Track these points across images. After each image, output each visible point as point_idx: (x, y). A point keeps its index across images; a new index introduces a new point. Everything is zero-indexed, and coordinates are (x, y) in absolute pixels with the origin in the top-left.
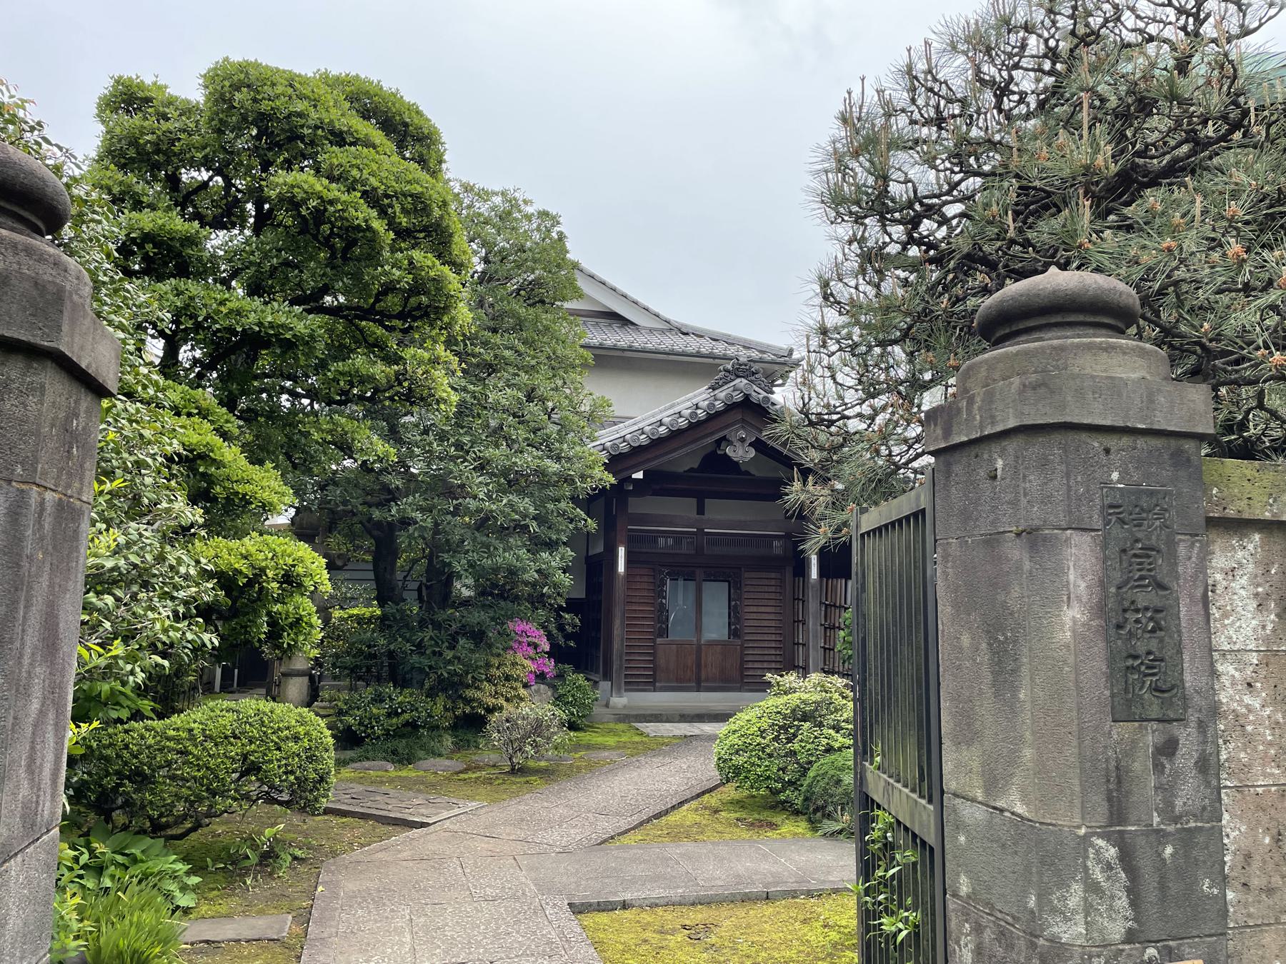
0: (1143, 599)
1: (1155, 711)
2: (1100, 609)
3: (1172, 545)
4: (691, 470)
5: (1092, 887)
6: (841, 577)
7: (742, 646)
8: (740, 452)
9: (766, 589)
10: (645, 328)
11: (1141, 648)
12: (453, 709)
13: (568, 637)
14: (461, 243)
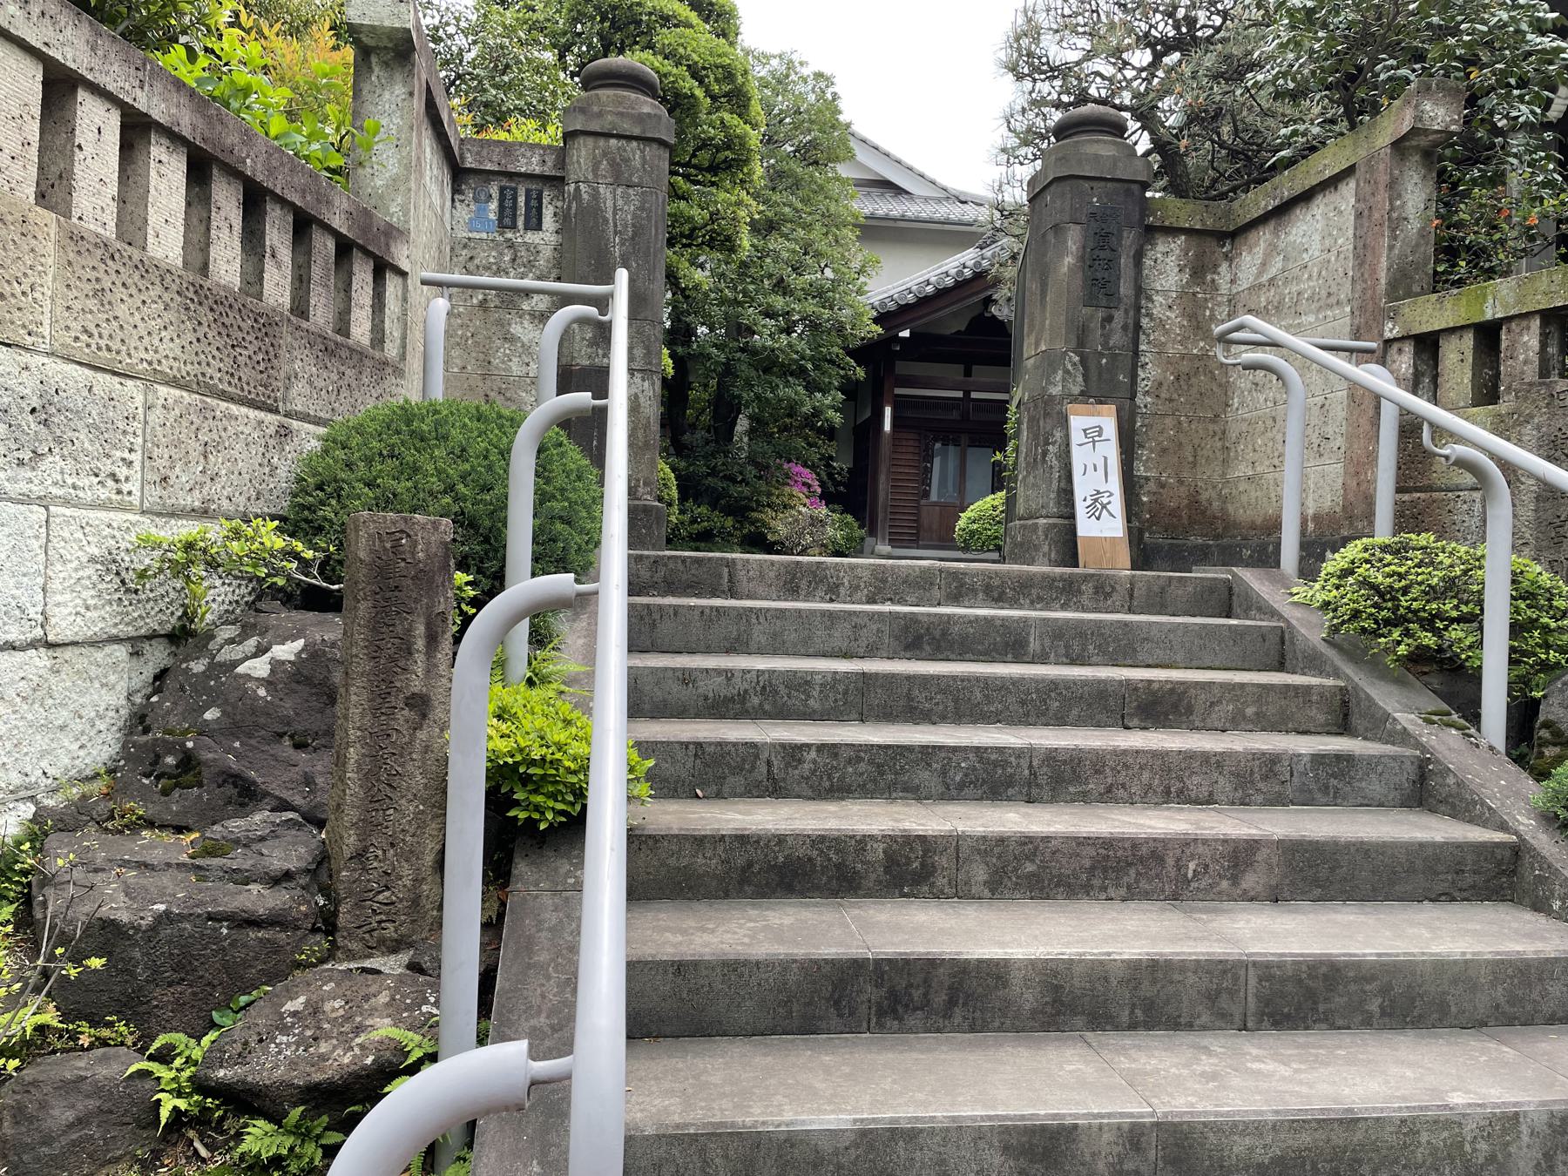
0: (1102, 254)
1: (1104, 303)
2: (1082, 258)
3: (1120, 231)
4: (959, 332)
5: (1067, 372)
10: (920, 197)
11: (1099, 275)
12: (742, 527)
13: (837, 484)
14: (756, 108)
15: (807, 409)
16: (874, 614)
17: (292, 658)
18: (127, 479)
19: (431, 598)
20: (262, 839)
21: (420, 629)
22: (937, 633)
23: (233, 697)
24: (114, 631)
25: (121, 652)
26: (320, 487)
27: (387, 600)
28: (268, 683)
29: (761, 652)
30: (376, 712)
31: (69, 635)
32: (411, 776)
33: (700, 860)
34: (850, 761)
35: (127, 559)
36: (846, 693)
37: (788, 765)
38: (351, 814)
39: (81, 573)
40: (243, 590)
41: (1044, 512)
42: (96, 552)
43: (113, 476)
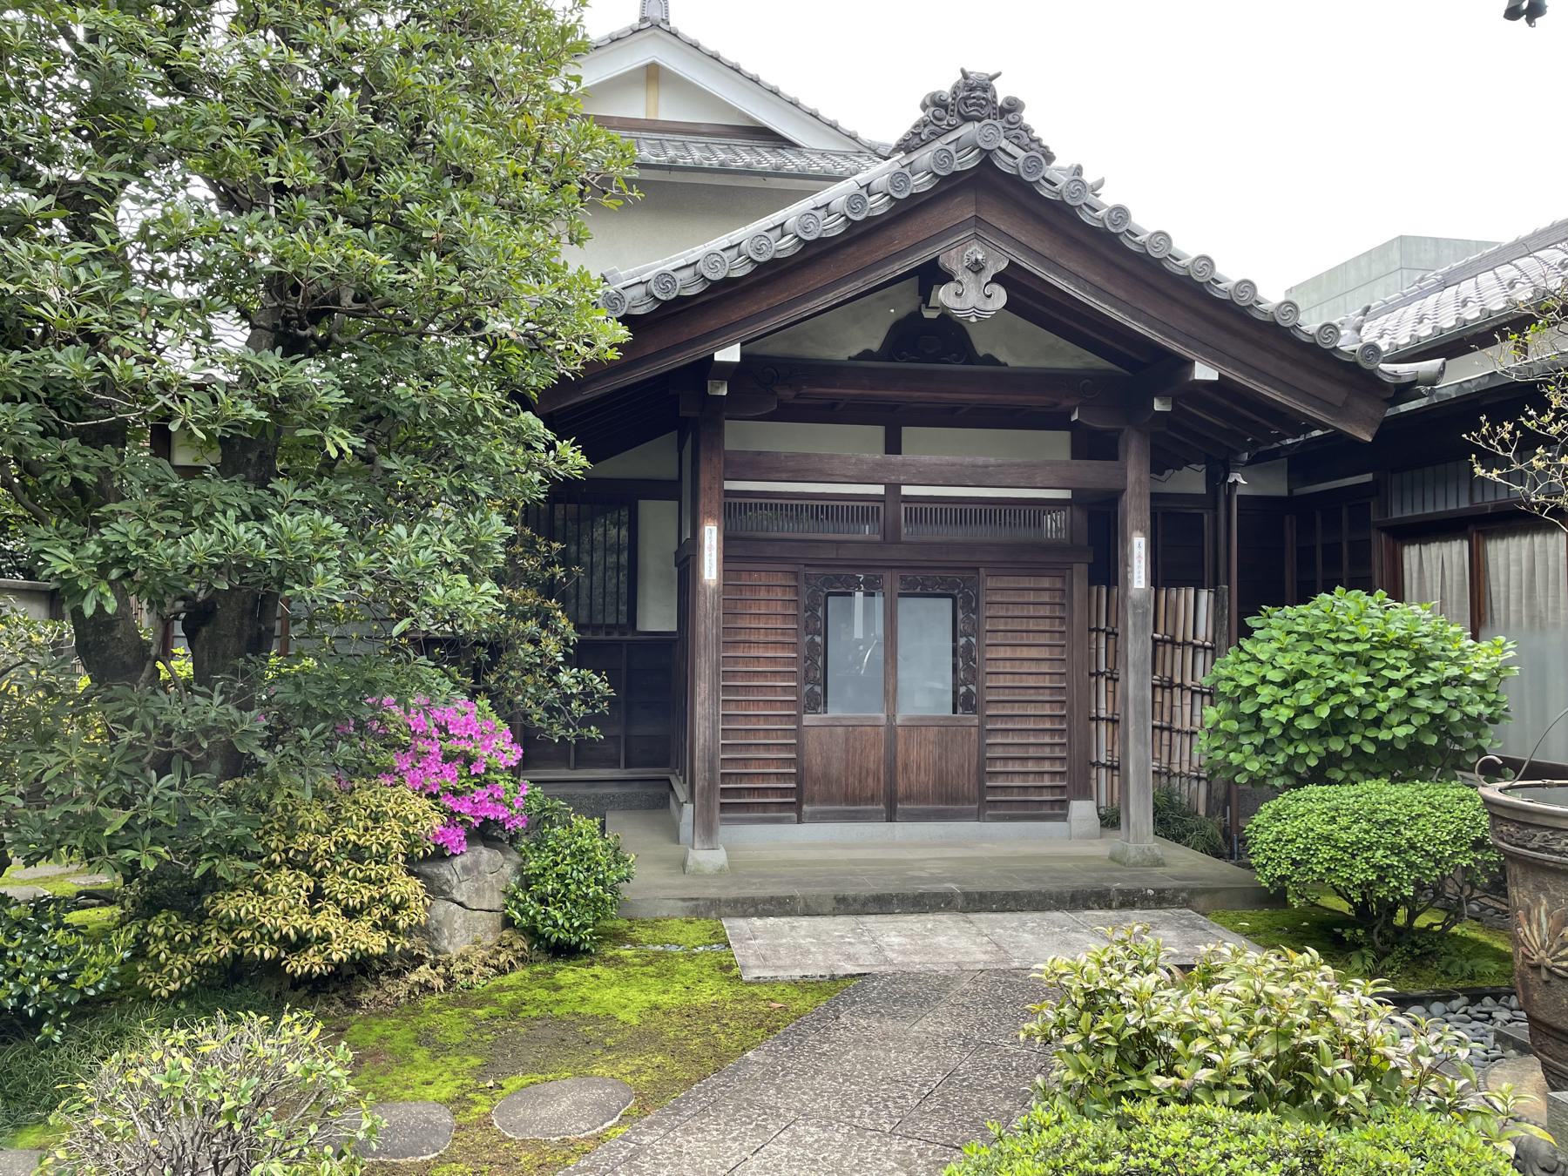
4: (866, 355)
6: (1186, 584)
7: (981, 727)
9: (1031, 611)
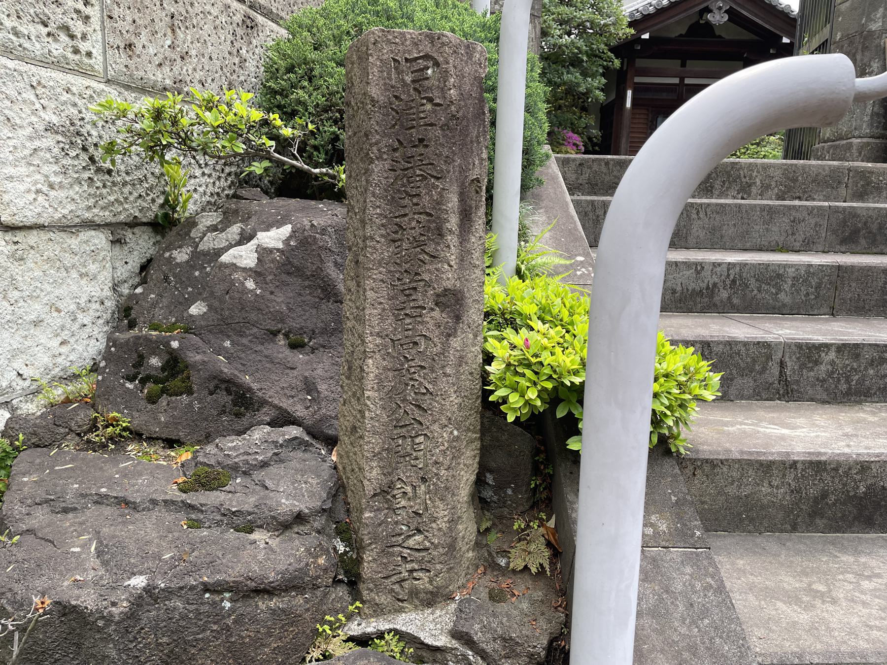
4: (681, 35)
8: (718, 17)
15: (583, 89)
16: (813, 208)
17: (280, 246)
18: (84, 37)
19: (464, 158)
20: (264, 465)
21: (453, 201)
22: (874, 227)
23: (219, 289)
24: (88, 215)
25: (100, 239)
26: (290, 69)
27: (408, 159)
28: (256, 273)
29: (699, 247)
30: (399, 313)
31: (29, 216)
32: (445, 396)
33: (765, 489)
34: (871, 363)
35: (94, 133)
36: (818, 287)
37: (803, 366)
38: (373, 443)
39: (37, 143)
40: (223, 183)
41: (857, 133)
42: (55, 120)
43: (66, 28)
